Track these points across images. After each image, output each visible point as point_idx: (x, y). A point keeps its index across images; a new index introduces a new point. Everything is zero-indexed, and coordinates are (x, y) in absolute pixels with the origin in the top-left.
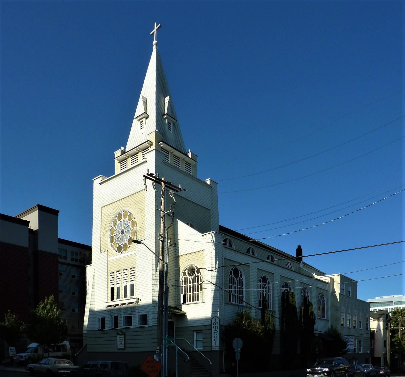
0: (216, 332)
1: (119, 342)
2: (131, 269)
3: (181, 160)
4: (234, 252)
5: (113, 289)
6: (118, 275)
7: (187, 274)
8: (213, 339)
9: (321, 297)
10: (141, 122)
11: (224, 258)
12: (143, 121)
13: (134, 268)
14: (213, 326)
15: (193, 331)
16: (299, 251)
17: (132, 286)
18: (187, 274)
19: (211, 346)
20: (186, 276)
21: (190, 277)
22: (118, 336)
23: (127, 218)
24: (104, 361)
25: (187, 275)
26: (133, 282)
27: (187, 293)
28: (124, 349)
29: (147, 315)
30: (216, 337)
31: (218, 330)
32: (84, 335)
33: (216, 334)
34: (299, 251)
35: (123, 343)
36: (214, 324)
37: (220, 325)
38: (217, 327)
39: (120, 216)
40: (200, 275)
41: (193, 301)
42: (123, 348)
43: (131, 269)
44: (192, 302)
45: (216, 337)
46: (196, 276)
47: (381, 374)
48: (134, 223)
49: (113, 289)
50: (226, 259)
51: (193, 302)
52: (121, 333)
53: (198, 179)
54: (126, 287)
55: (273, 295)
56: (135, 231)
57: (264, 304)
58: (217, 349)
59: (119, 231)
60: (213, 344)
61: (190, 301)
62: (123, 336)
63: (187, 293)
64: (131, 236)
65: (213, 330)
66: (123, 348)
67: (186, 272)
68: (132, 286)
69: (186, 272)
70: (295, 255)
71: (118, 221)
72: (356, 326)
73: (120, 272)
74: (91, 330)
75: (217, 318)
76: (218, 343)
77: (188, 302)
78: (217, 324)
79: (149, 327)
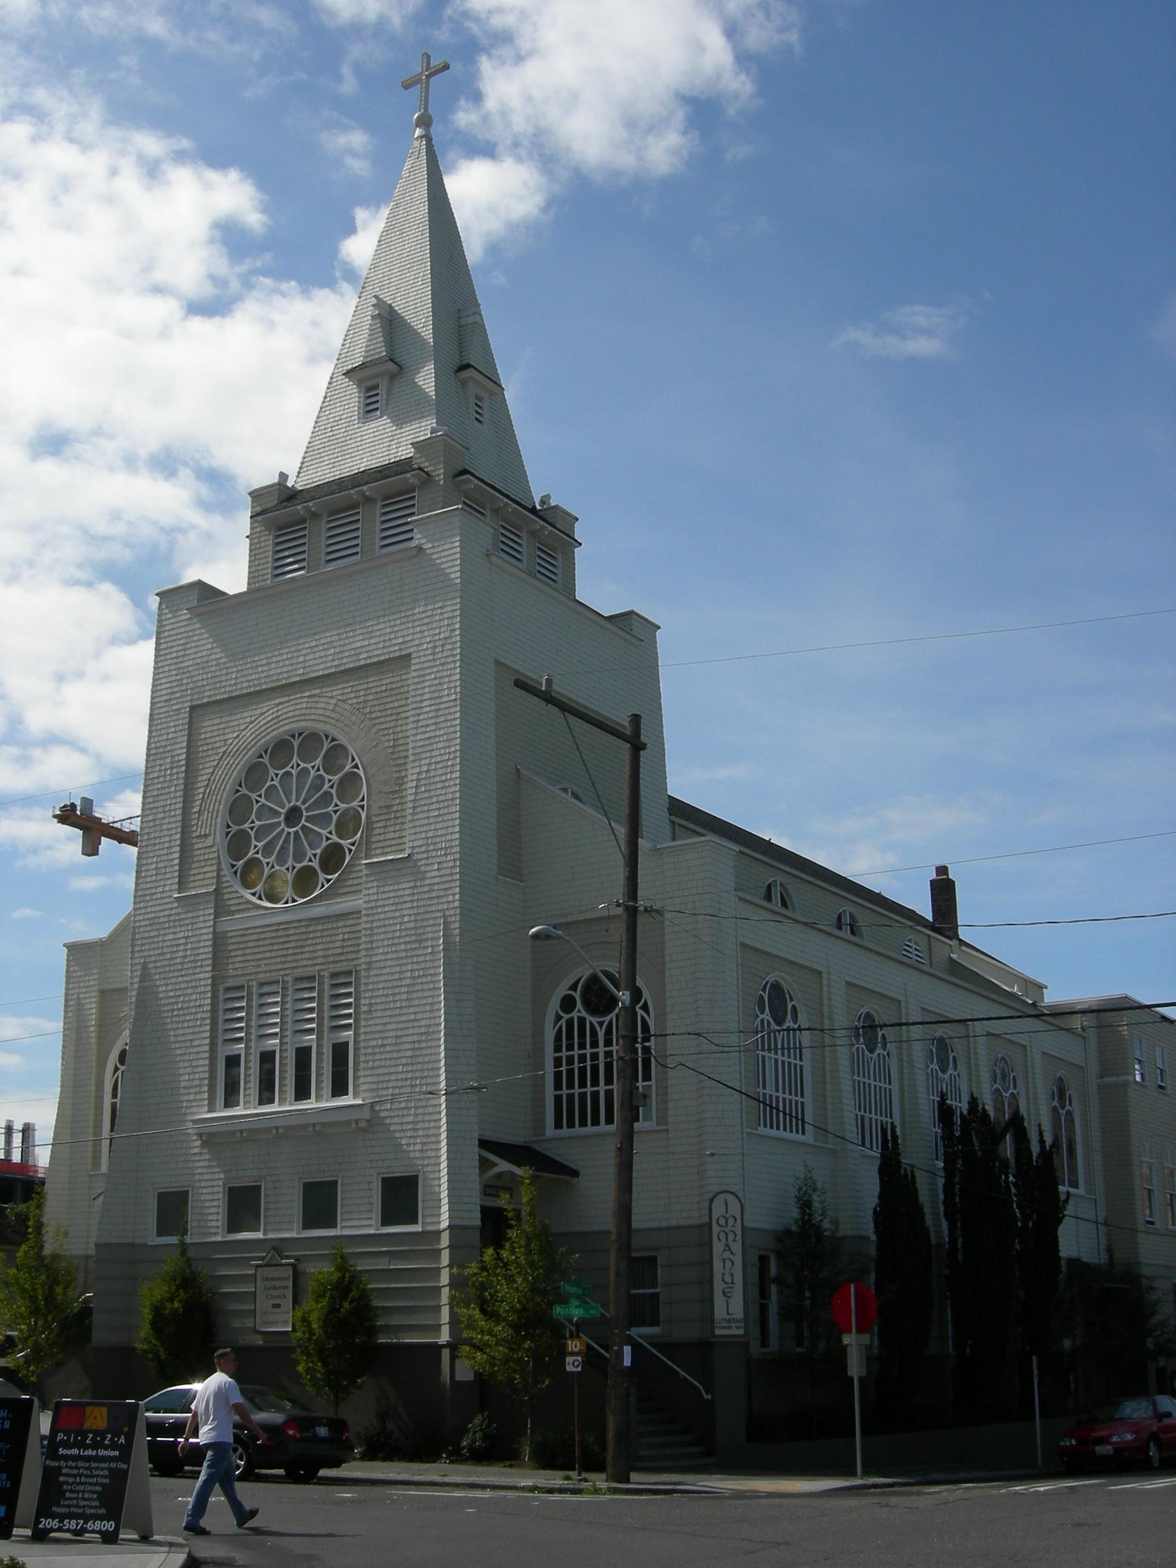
0: (727, 1255)
7: (579, 1005)
9: (1004, 1076)
10: (369, 389)
12: (376, 387)
16: (943, 890)
18: (579, 1005)
24: (69, 1453)
25: (579, 1011)
30: (728, 1279)
31: (737, 1247)
34: (943, 890)
36: (722, 1221)
37: (743, 1227)
40: (640, 1012)
45: (728, 1279)
50: (854, 985)
55: (902, 1090)
60: (720, 1312)
64: (335, 838)
65: (718, 1248)
68: (340, 1053)
70: (925, 909)
72: (1156, 1219)
75: (730, 1198)
76: (737, 1308)
78: (731, 1221)
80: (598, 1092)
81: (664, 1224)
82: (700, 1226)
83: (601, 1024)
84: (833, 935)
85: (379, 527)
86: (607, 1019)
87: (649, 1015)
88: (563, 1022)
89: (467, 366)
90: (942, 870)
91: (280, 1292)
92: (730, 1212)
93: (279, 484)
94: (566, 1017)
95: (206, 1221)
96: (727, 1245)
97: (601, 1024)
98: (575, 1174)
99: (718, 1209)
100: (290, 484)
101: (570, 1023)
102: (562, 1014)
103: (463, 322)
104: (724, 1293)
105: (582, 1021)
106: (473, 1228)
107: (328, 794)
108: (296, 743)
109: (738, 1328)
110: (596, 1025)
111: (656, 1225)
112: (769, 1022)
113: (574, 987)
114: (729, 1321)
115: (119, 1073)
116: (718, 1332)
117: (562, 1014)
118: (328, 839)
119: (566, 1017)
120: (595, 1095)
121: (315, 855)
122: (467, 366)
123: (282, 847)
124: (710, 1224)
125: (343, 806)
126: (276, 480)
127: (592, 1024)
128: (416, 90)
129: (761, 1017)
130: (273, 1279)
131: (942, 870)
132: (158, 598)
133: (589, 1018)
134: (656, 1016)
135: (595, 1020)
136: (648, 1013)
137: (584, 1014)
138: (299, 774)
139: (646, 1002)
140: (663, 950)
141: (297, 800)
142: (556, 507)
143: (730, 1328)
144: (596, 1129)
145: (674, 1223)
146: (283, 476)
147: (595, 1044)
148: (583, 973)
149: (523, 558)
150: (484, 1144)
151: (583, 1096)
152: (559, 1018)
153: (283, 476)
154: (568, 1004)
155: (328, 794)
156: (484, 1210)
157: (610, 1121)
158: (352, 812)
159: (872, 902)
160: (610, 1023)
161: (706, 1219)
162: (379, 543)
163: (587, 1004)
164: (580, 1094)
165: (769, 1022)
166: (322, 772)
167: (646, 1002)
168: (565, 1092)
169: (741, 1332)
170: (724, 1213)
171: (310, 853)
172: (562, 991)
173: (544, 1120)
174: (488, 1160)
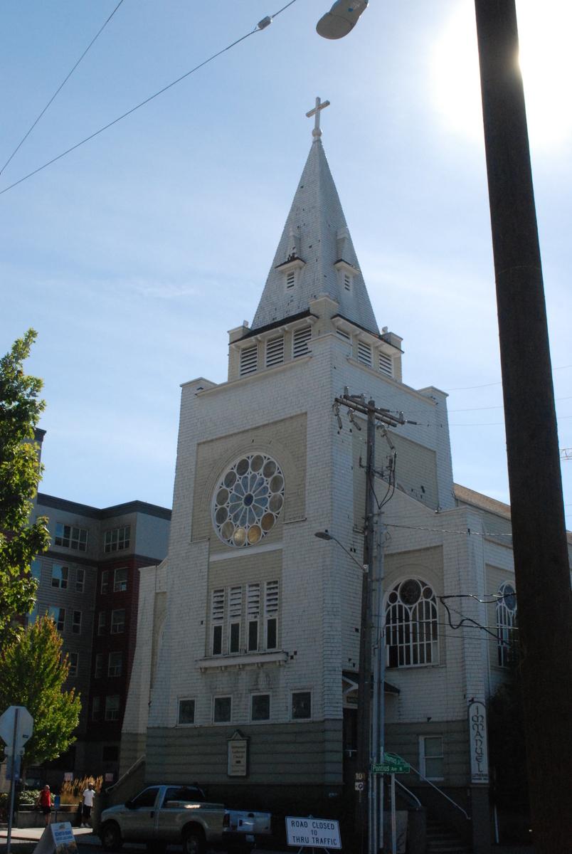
0: (478, 738)
1: (231, 760)
2: (269, 584)
3: (372, 349)
4: (504, 548)
5: (218, 631)
6: (234, 597)
7: (399, 599)
8: (473, 755)
11: (487, 565)
12: (293, 274)
13: (257, 585)
14: (471, 723)
15: (418, 735)
17: (272, 624)
18: (399, 599)
19: (469, 772)
20: (397, 603)
21: (405, 606)
22: (230, 744)
23: (261, 471)
25: (399, 602)
26: (275, 616)
27: (401, 642)
28: (246, 777)
29: (310, 693)
30: (479, 751)
32: (123, 738)
33: (479, 743)
35: (244, 761)
36: (475, 719)
38: (480, 727)
39: (243, 467)
40: (431, 602)
41: (415, 662)
42: (244, 774)
43: (269, 584)
44: (405, 666)
46: (421, 604)
47: (530, 833)
48: (277, 483)
49: (218, 631)
50: (490, 565)
51: (423, 665)
52: (239, 737)
53: (347, 405)
54: (235, 628)
56: (280, 501)
57: (76, 695)
58: (483, 781)
59: (239, 499)
60: (474, 770)
61: (402, 664)
62: (243, 743)
63: (401, 642)
65: (473, 733)
66: (244, 774)
67: (398, 593)
68: (272, 624)
69: (398, 593)
71: (238, 476)
73: (239, 591)
74: (159, 728)
75: (479, 705)
76: (484, 767)
77: (402, 664)
78: (480, 719)
79: (313, 722)
80: (409, 646)
81: (445, 719)
82: (463, 721)
83: (410, 609)
85: (293, 351)
86: (414, 606)
88: (391, 608)
89: (341, 260)
91: (240, 754)
92: (480, 714)
93: (244, 327)
94: (392, 605)
96: (478, 732)
98: (398, 691)
99: (472, 711)
100: (249, 326)
102: (390, 603)
103: (338, 238)
104: (477, 759)
105: (400, 607)
106: (340, 720)
107: (265, 499)
108: (250, 461)
109: (485, 779)
111: (440, 720)
112: (505, 608)
113: (396, 589)
114: (480, 775)
116: (473, 781)
117: (390, 603)
118: (266, 511)
119: (392, 605)
120: (408, 648)
121: (259, 520)
122: (341, 260)
123: (243, 516)
124: (468, 720)
125: (273, 494)
126: (242, 324)
127: (406, 609)
128: (313, 117)
129: (500, 604)
130: (236, 747)
132: (181, 388)
133: (404, 605)
137: (401, 603)
138: (251, 478)
139: (434, 597)
140: (442, 568)
141: (250, 491)
142: (390, 333)
143: (480, 779)
145: (449, 719)
146: (246, 323)
148: (402, 580)
149: (372, 365)
150: (345, 673)
151: (401, 627)
152: (389, 605)
153: (246, 323)
154: (393, 598)
155: (265, 499)
156: (345, 711)
158: (278, 496)
160: (416, 608)
161: (467, 717)
162: (293, 355)
163: (403, 598)
164: (402, 622)
165: (505, 608)
166: (263, 476)
167: (434, 597)
168: (391, 625)
169: (487, 782)
170: (476, 714)
171: (257, 519)
172: (390, 590)
174: (348, 683)
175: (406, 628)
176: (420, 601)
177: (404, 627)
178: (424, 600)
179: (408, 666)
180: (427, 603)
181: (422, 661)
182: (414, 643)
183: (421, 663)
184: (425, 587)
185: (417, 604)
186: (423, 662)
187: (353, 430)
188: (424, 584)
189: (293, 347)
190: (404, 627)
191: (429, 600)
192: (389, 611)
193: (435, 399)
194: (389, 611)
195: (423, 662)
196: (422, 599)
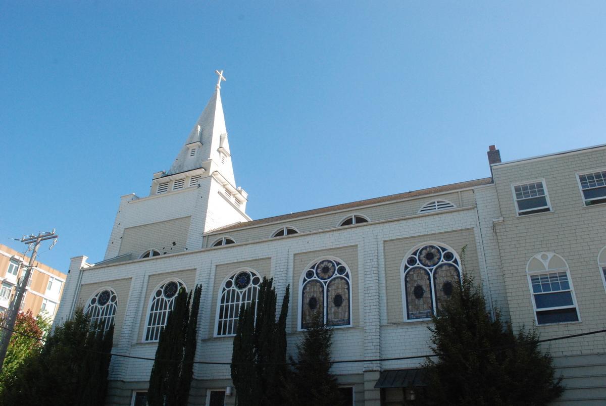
25: (163, 296)
41: (224, 333)
46: (250, 289)
67: (233, 281)
69: (233, 281)
83: (101, 308)
84: (143, 261)
86: (104, 307)
87: (349, 278)
90: (492, 148)
94: (227, 289)
95: (120, 342)
97: (169, 301)
101: (229, 292)
105: (234, 291)
110: (239, 293)
113: (232, 278)
115: (226, 291)
117: (156, 297)
119: (227, 289)
127: (237, 292)
131: (492, 148)
133: (165, 298)
134: (352, 278)
135: (167, 299)
136: (116, 305)
137: (164, 297)
139: (347, 273)
144: (151, 341)
147: (238, 300)
157: (156, 339)
159: (323, 212)
162: (173, 188)
163: (236, 284)
167: (116, 302)
173: (214, 325)
175: (226, 308)
176: (249, 286)
177: (235, 301)
178: (253, 286)
179: (151, 341)
180: (112, 305)
181: (224, 333)
182: (226, 319)
183: (228, 334)
184: (444, 252)
185: (247, 289)
186: (220, 334)
187: (120, 226)
188: (254, 274)
189: (190, 182)
190: (235, 301)
191: (113, 303)
192: (224, 295)
193: (498, 151)
194: (224, 295)
195: (220, 334)
196: (110, 302)
